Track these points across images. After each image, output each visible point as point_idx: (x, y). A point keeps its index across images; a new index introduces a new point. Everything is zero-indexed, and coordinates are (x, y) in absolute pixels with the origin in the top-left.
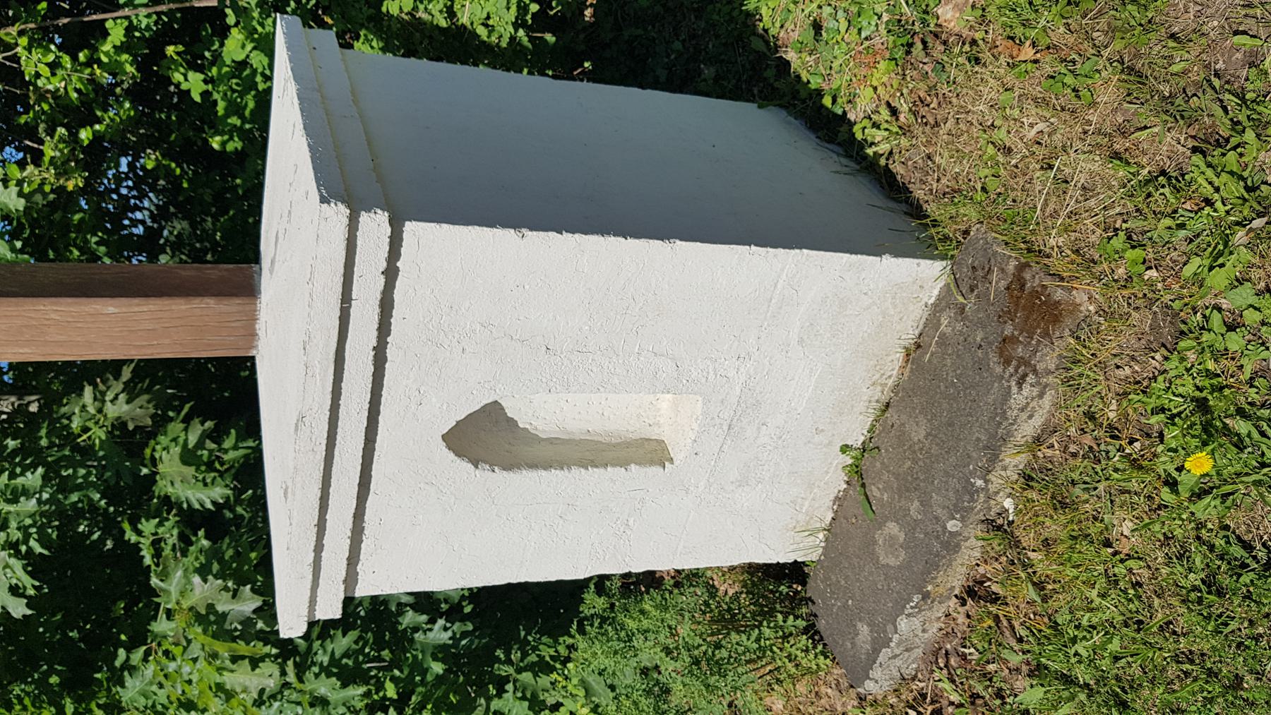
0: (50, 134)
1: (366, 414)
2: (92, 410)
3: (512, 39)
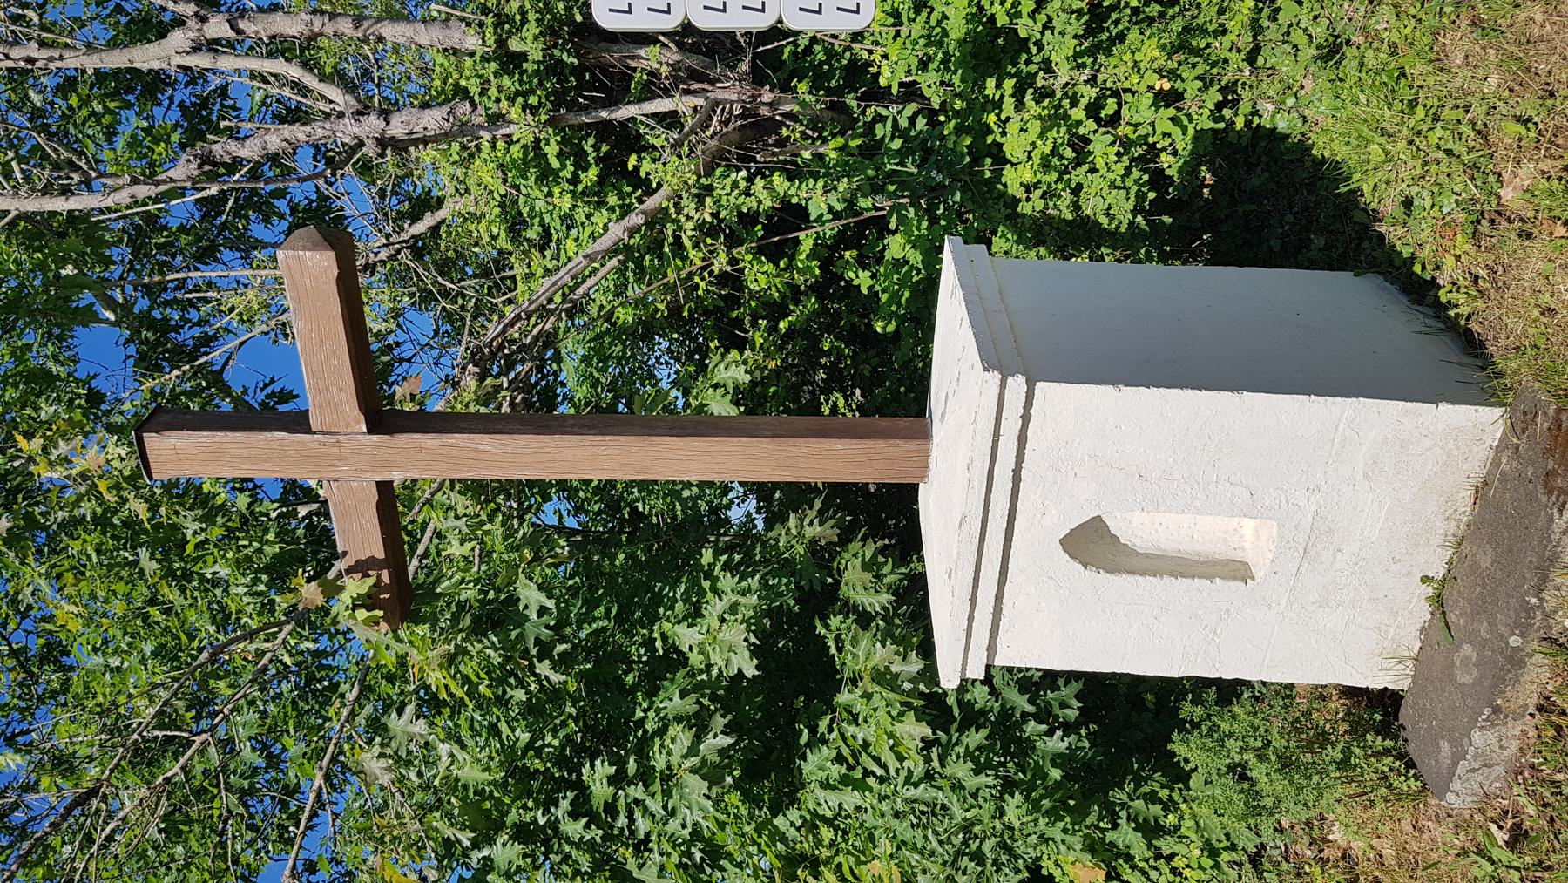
0: (754, 324)
2: (794, 532)
3: (1131, 223)
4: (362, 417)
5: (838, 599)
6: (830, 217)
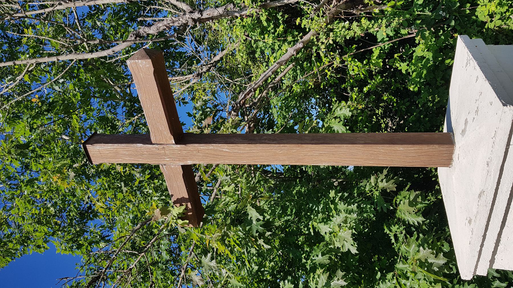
0: (352, 90)
1: (509, 192)
4: (172, 137)
5: (396, 217)
6: (388, 39)
